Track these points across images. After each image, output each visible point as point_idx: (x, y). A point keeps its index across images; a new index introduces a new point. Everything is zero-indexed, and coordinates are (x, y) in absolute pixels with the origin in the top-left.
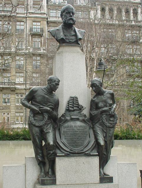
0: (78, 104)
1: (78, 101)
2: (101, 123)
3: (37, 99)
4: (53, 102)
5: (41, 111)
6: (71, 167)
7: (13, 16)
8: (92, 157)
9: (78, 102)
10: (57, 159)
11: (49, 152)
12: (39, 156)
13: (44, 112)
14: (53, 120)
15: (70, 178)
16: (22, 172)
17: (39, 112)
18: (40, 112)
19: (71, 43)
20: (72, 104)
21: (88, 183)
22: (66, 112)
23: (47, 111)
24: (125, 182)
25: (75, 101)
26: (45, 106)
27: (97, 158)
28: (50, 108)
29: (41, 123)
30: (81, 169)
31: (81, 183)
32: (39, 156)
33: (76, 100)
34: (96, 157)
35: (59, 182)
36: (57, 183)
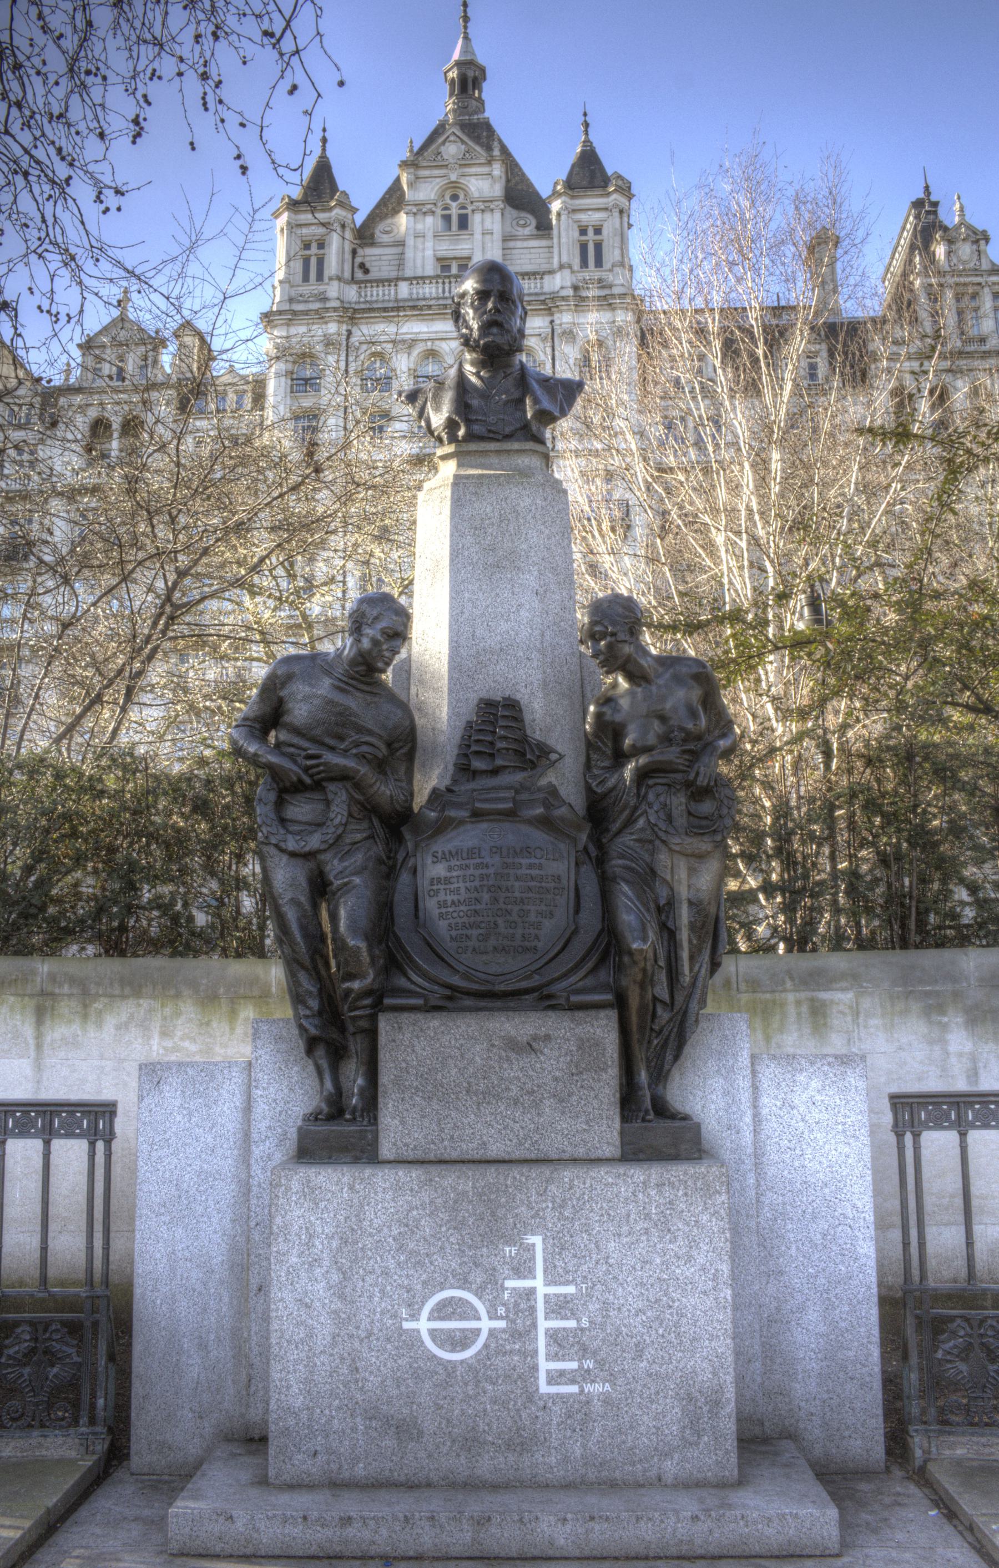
0: (524, 740)
1: (522, 721)
2: (643, 830)
3: (297, 712)
4: (376, 730)
5: (311, 776)
6: (461, 1065)
7: (780, 574)
8: (580, 1015)
9: (522, 729)
10: (385, 1024)
11: (347, 985)
12: (308, 1012)
13: (332, 779)
14: (382, 821)
15: (456, 1127)
16: (234, 1095)
17: (300, 781)
18: (308, 780)
19: (498, 440)
20: (489, 738)
21: (557, 1157)
22: (455, 781)
23: (344, 777)
24: (797, 1164)
25: (501, 723)
26: (332, 749)
27: (608, 1018)
28: (362, 757)
29: (314, 842)
30: (518, 1078)
31: (517, 1155)
32: (308, 1012)
33: (515, 719)
34: (602, 1014)
35: (395, 1144)
36: (107, 1095)
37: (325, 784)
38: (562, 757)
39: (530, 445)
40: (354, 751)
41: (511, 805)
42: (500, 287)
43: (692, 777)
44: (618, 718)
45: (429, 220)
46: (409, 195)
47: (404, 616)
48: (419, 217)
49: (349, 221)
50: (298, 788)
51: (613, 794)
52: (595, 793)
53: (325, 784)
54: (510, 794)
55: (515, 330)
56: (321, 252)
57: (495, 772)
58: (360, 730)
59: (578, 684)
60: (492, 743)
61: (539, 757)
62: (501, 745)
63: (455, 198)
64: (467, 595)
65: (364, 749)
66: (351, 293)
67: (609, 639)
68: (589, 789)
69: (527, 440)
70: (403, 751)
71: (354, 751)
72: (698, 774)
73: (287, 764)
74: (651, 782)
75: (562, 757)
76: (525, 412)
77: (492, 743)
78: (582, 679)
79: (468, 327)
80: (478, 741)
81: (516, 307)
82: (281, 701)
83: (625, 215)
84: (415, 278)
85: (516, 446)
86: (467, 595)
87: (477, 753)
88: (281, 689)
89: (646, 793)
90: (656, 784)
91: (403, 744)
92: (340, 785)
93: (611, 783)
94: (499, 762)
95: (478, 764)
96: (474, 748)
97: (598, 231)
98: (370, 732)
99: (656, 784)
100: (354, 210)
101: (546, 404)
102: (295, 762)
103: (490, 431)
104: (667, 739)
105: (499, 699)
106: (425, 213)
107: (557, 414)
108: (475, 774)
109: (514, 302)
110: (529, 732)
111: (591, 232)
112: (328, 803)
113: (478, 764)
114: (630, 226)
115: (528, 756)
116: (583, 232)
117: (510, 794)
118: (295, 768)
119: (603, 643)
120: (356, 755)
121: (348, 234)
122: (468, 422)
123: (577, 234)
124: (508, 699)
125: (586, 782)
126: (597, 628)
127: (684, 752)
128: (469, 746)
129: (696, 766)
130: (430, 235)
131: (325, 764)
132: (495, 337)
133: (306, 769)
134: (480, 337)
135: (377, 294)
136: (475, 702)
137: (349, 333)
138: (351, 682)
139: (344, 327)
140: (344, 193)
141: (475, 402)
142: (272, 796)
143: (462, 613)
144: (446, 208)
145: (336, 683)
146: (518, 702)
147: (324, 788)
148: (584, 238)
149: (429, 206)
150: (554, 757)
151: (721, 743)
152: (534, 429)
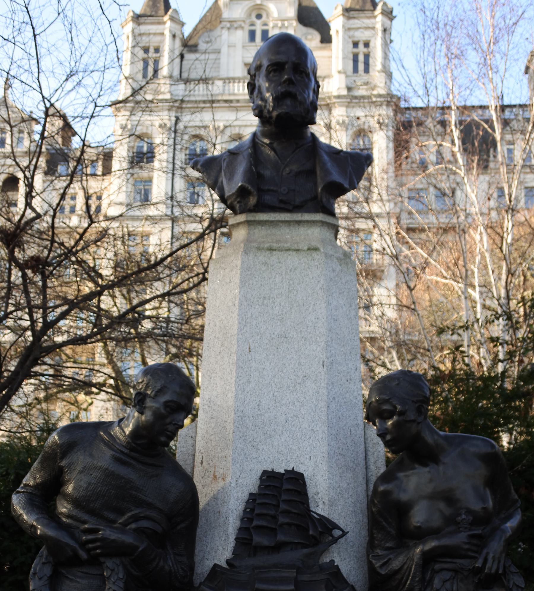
5: (88, 551)
17: (76, 555)
18: (83, 555)
20: (272, 512)
37: (102, 559)
38: (344, 533)
39: (319, 217)
40: (133, 526)
41: (292, 587)
42: (294, 59)
43: (479, 564)
44: (404, 497)
45: (239, 33)
46: (226, 15)
47: (190, 390)
48: (232, 31)
49: (178, 33)
50: (74, 561)
51: (399, 576)
52: (379, 574)
53: (102, 559)
54: (293, 573)
55: (308, 102)
56: (158, 55)
57: (278, 547)
58: (141, 503)
59: (362, 456)
60: (274, 517)
61: (321, 533)
62: (282, 520)
63: (259, 16)
64: (253, 364)
65: (145, 524)
66: (180, 89)
67: (395, 418)
68: (372, 570)
69: (316, 211)
70: (183, 525)
71: (133, 526)
72: (486, 561)
73: (66, 539)
74: (437, 566)
75: (344, 533)
76: (316, 184)
77: (274, 517)
78: (366, 451)
79: (263, 99)
80: (259, 515)
81: (310, 80)
82: (61, 471)
83: (387, 32)
84: (229, 79)
85: (307, 217)
86: (253, 364)
87: (259, 528)
88: (62, 458)
89: (431, 579)
90: (442, 570)
91: (184, 513)
92: (117, 561)
93: (396, 564)
94: (281, 538)
95: (258, 539)
96: (255, 523)
97: (367, 45)
98: (150, 506)
99: (442, 570)
100: (183, 24)
101: (336, 177)
102: (73, 536)
103: (281, 201)
104: (451, 521)
105: (282, 471)
106: (236, 28)
107: (346, 186)
108: (257, 550)
109: (308, 75)
110: (312, 507)
111: (361, 46)
112: (104, 580)
113: (258, 539)
114: (391, 41)
115: (311, 532)
116: (356, 44)
117: (293, 573)
118: (72, 543)
119: (390, 423)
120: (135, 530)
121: (178, 43)
122: (260, 191)
123: (351, 45)
124: (293, 472)
125: (370, 563)
126: (386, 407)
127: (472, 536)
128: (251, 520)
129: (485, 551)
130: (239, 45)
131: (103, 539)
132: (287, 106)
133: (83, 545)
134: (274, 108)
135: (200, 92)
136: (259, 474)
137: (178, 119)
138: (133, 454)
139: (173, 114)
140: (175, 11)
141: (267, 173)
142: (48, 571)
143: (249, 382)
144: (252, 24)
145: (118, 455)
146: (302, 475)
147: (101, 564)
148: (355, 50)
149: (239, 23)
150: (337, 533)
151: (508, 524)
152: (324, 200)
